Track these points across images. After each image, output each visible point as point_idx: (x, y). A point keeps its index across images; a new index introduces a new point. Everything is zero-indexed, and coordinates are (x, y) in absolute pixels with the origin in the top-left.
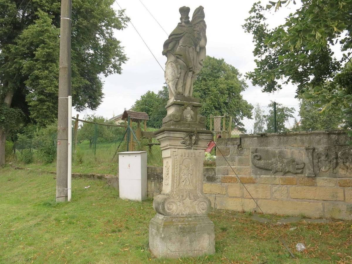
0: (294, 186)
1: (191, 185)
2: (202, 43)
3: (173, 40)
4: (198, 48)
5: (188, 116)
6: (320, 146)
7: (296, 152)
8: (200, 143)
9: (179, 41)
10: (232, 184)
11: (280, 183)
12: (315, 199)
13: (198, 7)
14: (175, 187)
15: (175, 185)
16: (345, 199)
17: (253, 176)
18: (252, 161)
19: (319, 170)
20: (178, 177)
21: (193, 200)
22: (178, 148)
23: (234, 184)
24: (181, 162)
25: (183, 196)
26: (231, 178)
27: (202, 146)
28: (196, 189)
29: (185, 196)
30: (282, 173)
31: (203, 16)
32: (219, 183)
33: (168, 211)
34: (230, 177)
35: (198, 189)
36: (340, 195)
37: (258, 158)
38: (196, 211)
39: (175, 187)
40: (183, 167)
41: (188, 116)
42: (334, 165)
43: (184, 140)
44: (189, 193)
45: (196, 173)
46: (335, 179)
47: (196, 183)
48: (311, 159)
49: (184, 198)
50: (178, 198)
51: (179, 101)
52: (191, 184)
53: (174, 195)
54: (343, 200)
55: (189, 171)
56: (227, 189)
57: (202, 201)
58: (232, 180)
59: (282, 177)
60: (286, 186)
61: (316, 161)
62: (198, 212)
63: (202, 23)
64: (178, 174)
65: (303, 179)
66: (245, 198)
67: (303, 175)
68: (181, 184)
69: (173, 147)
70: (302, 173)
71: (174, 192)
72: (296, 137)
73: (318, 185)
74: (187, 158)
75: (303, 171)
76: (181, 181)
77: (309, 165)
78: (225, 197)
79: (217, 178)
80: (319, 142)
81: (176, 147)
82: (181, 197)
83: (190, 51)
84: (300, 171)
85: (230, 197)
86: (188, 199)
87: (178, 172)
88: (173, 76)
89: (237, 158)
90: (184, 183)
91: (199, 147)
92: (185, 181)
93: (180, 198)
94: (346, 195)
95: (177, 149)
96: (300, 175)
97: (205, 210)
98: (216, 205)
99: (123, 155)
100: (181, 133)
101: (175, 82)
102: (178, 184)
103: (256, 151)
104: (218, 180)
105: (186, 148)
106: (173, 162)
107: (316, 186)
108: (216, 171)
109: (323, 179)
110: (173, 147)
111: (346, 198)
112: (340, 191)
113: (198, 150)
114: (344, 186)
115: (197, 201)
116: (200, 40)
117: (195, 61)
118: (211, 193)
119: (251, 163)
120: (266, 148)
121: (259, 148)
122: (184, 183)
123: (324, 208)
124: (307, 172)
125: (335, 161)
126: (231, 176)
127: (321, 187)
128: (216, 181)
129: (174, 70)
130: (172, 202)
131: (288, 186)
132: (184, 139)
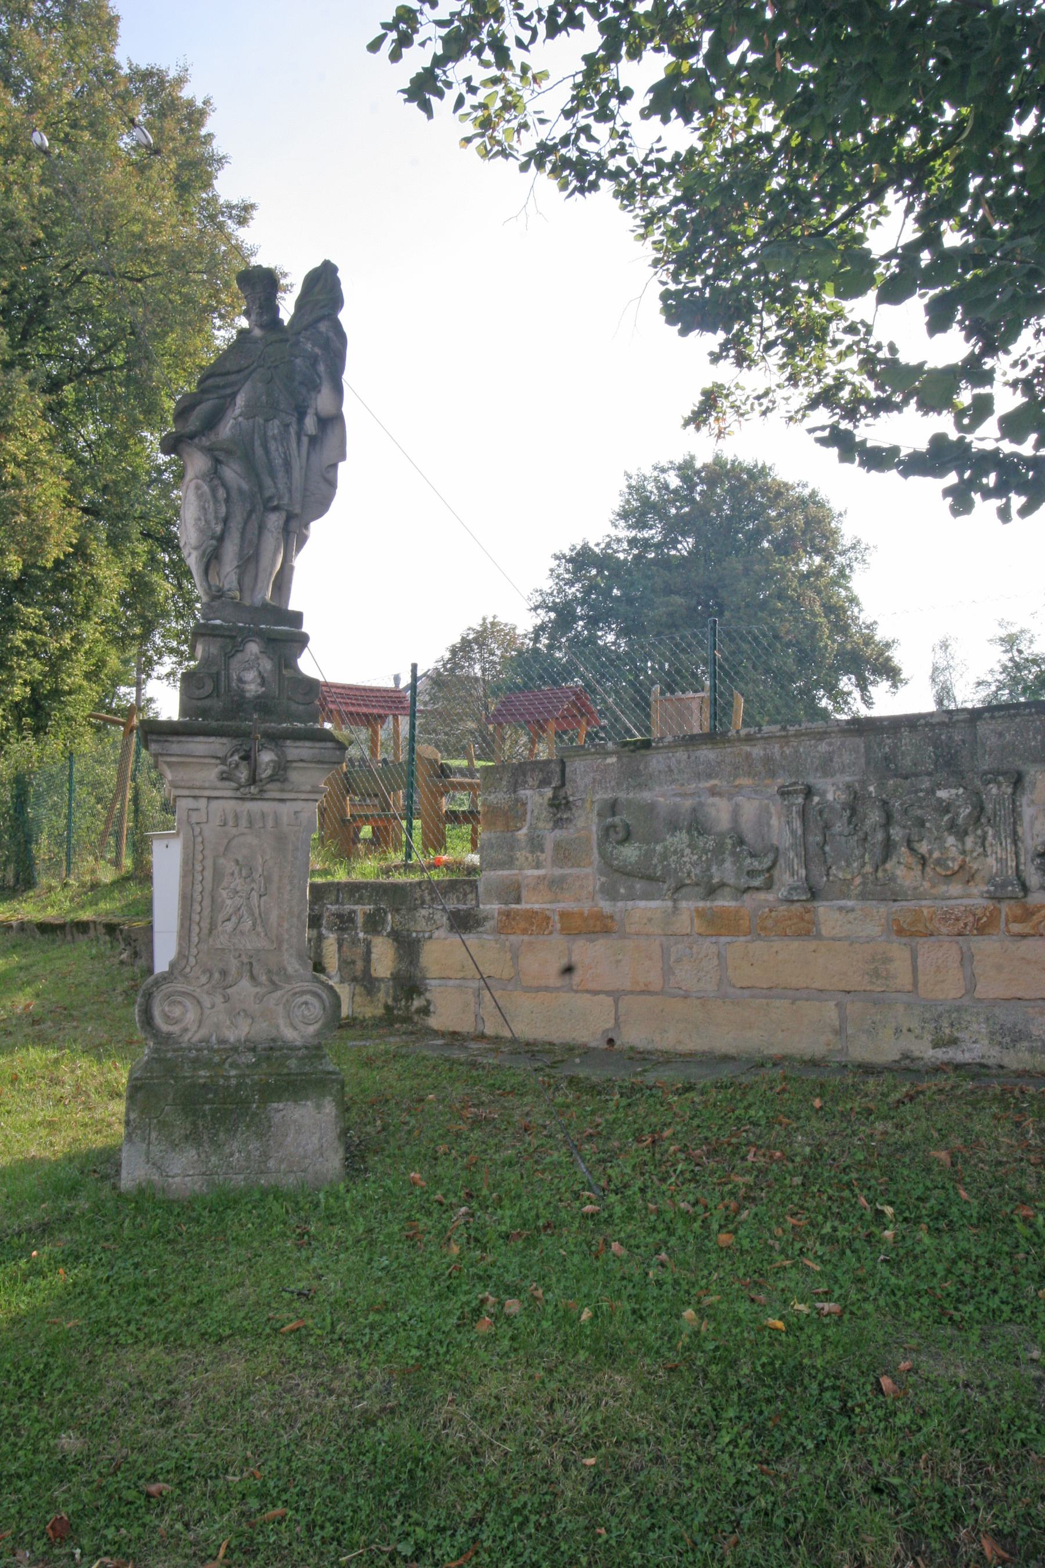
0: (742, 939)
1: (258, 935)
2: (323, 401)
3: (206, 396)
4: (310, 423)
5: (250, 676)
6: (829, 780)
7: (749, 808)
8: (294, 776)
9: (234, 396)
10: (532, 938)
11: (696, 929)
12: (814, 986)
13: (318, 264)
14: (195, 939)
15: (195, 929)
16: (915, 983)
17: (605, 906)
18: (599, 846)
19: (828, 875)
20: (207, 902)
21: (265, 990)
22: (209, 798)
23: (541, 937)
24: (222, 849)
25: (224, 973)
26: (531, 916)
27: (303, 788)
28: (279, 948)
29: (233, 971)
30: (701, 890)
31: (336, 301)
32: (490, 937)
33: (165, 1028)
34: (527, 911)
35: (285, 946)
36: (900, 967)
37: (621, 835)
38: (278, 1026)
39: (195, 939)
40: (230, 866)
41: (250, 676)
42: (878, 850)
43: (225, 768)
44: (251, 964)
45: (279, 888)
46: (883, 909)
47: (280, 925)
48: (800, 832)
49: (230, 979)
50: (204, 979)
51: (218, 622)
52: (259, 929)
53: (188, 969)
54: (909, 987)
55: (253, 881)
56: (515, 957)
57: (303, 993)
58: (532, 924)
59: (701, 904)
60: (714, 939)
61: (815, 838)
62: (290, 1034)
63: (323, 327)
64: (206, 894)
65: (771, 911)
66: (577, 992)
67: (770, 897)
68: (220, 929)
69: (186, 792)
70: (769, 886)
71: (192, 961)
72: (748, 749)
73: (824, 932)
74: (243, 834)
75: (771, 878)
76: (221, 917)
77: (792, 854)
78: (510, 988)
79: (485, 919)
80: (826, 767)
81: (197, 792)
82: (217, 975)
83: (270, 433)
84: (757, 882)
85: (528, 989)
86: (245, 983)
87: (208, 885)
88: (201, 531)
89: (551, 837)
90: (229, 926)
91: (291, 791)
92: (234, 919)
93: (213, 982)
94: (920, 968)
95: (202, 803)
96: (762, 896)
97: (317, 1026)
98: (480, 1021)
99: (165, 842)
100: (212, 739)
101: (204, 552)
102: (205, 931)
103: (613, 807)
104: (489, 925)
105: (238, 794)
106: (185, 847)
107: (819, 936)
108: (481, 889)
109: (841, 909)
110: (186, 792)
111: (922, 978)
112: (899, 952)
113: (288, 803)
114: (912, 935)
115: (279, 993)
116: (316, 388)
117: (297, 474)
118: (462, 974)
119: (595, 855)
120: (647, 796)
121: (622, 795)
122: (229, 926)
123: (843, 1019)
124: (786, 879)
125: (880, 836)
126: (529, 906)
127: (833, 939)
128: (481, 929)
129: (204, 508)
130: (184, 994)
131: (723, 940)
132: (224, 763)
